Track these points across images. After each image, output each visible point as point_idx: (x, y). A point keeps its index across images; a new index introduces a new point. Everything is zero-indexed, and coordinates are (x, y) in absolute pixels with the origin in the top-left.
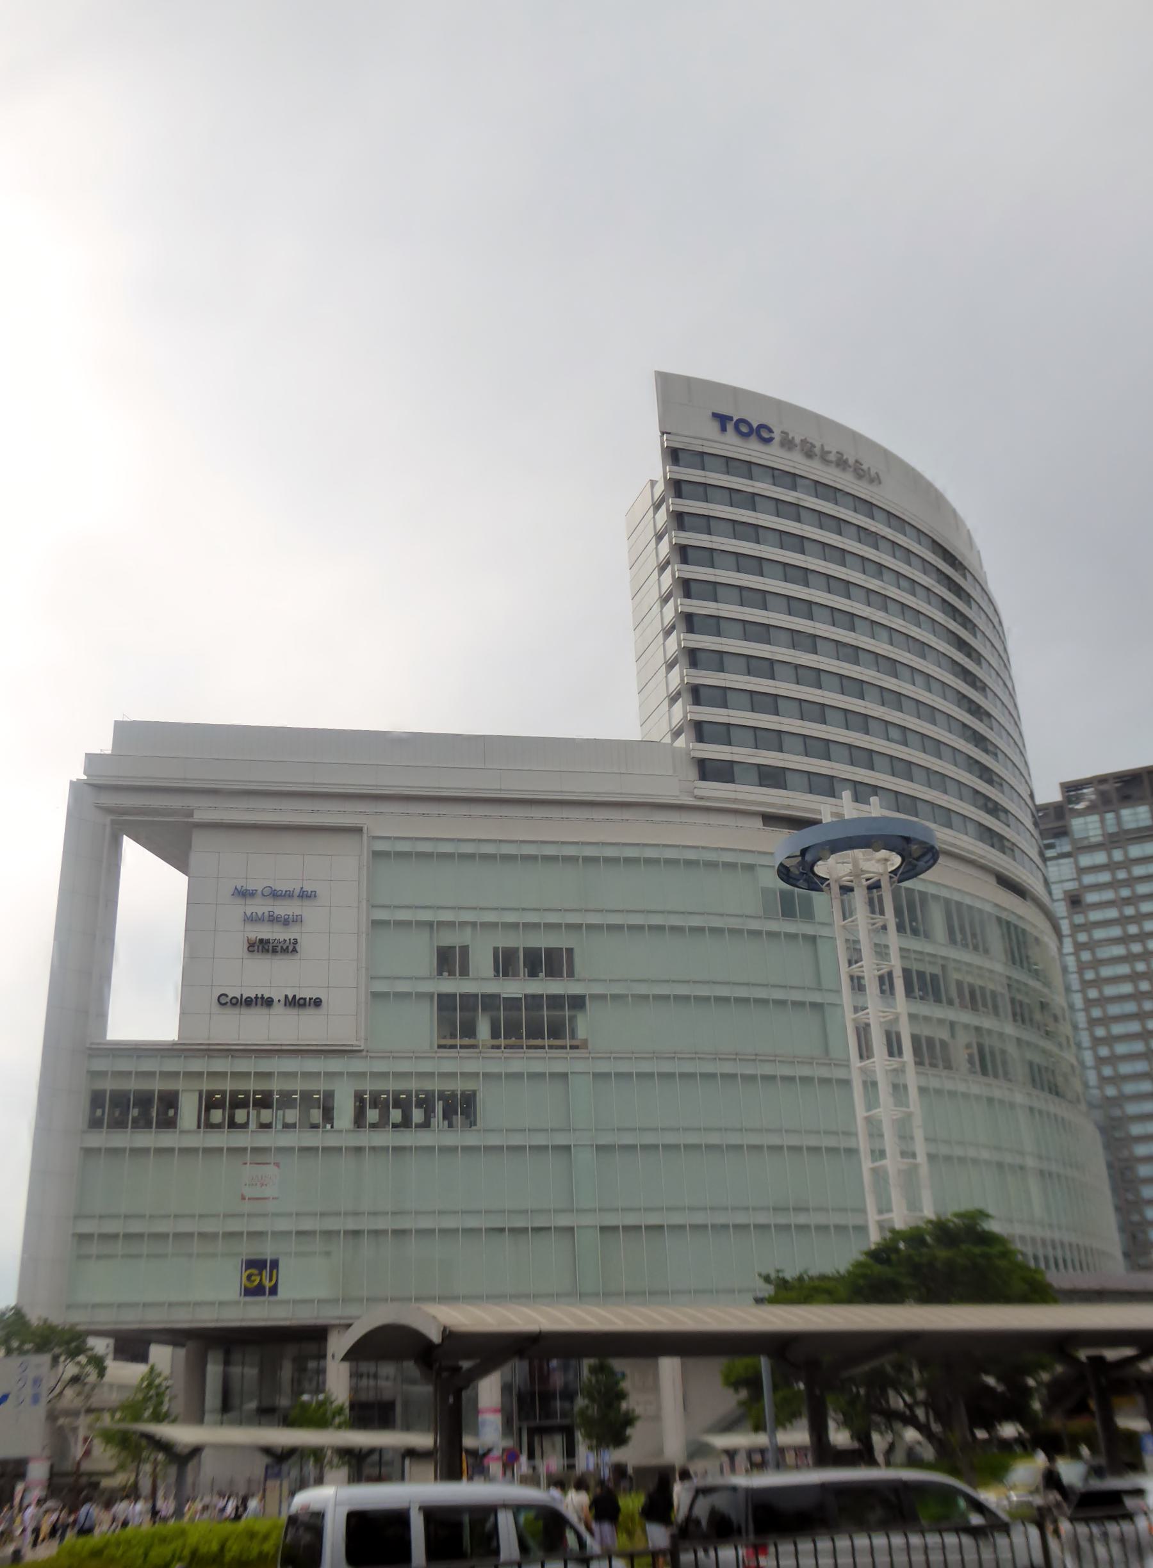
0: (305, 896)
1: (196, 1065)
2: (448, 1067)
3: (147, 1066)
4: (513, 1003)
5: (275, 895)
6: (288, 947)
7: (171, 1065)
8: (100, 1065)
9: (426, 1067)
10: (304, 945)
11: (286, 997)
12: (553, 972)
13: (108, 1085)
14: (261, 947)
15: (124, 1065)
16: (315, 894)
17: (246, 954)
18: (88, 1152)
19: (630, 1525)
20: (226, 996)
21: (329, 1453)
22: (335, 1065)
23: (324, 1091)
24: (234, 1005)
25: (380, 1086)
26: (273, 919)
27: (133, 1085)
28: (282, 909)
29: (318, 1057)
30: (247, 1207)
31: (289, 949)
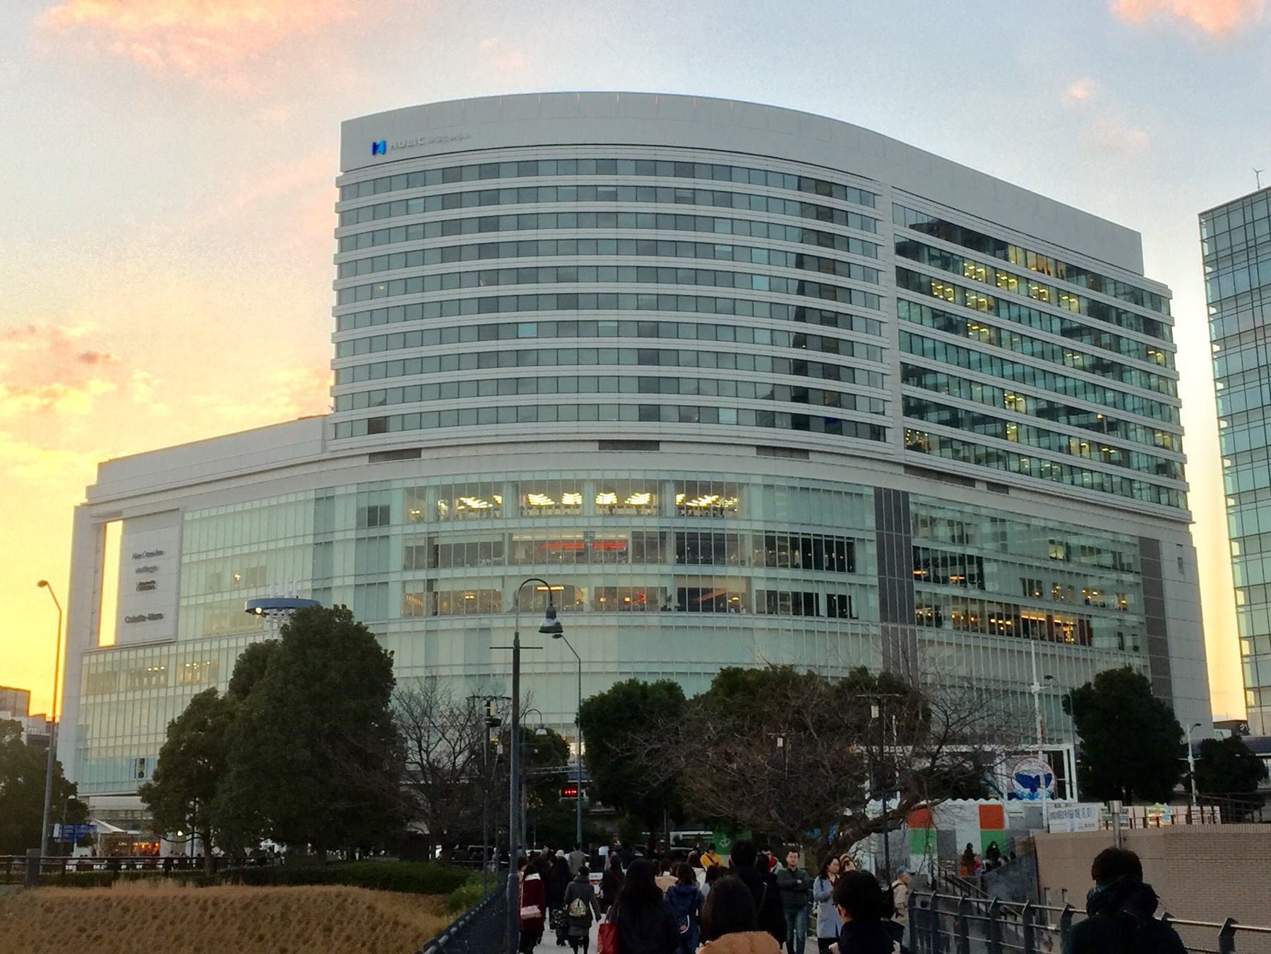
0: (160, 553)
5: (149, 555)
10: (159, 586)
19: (197, 515)
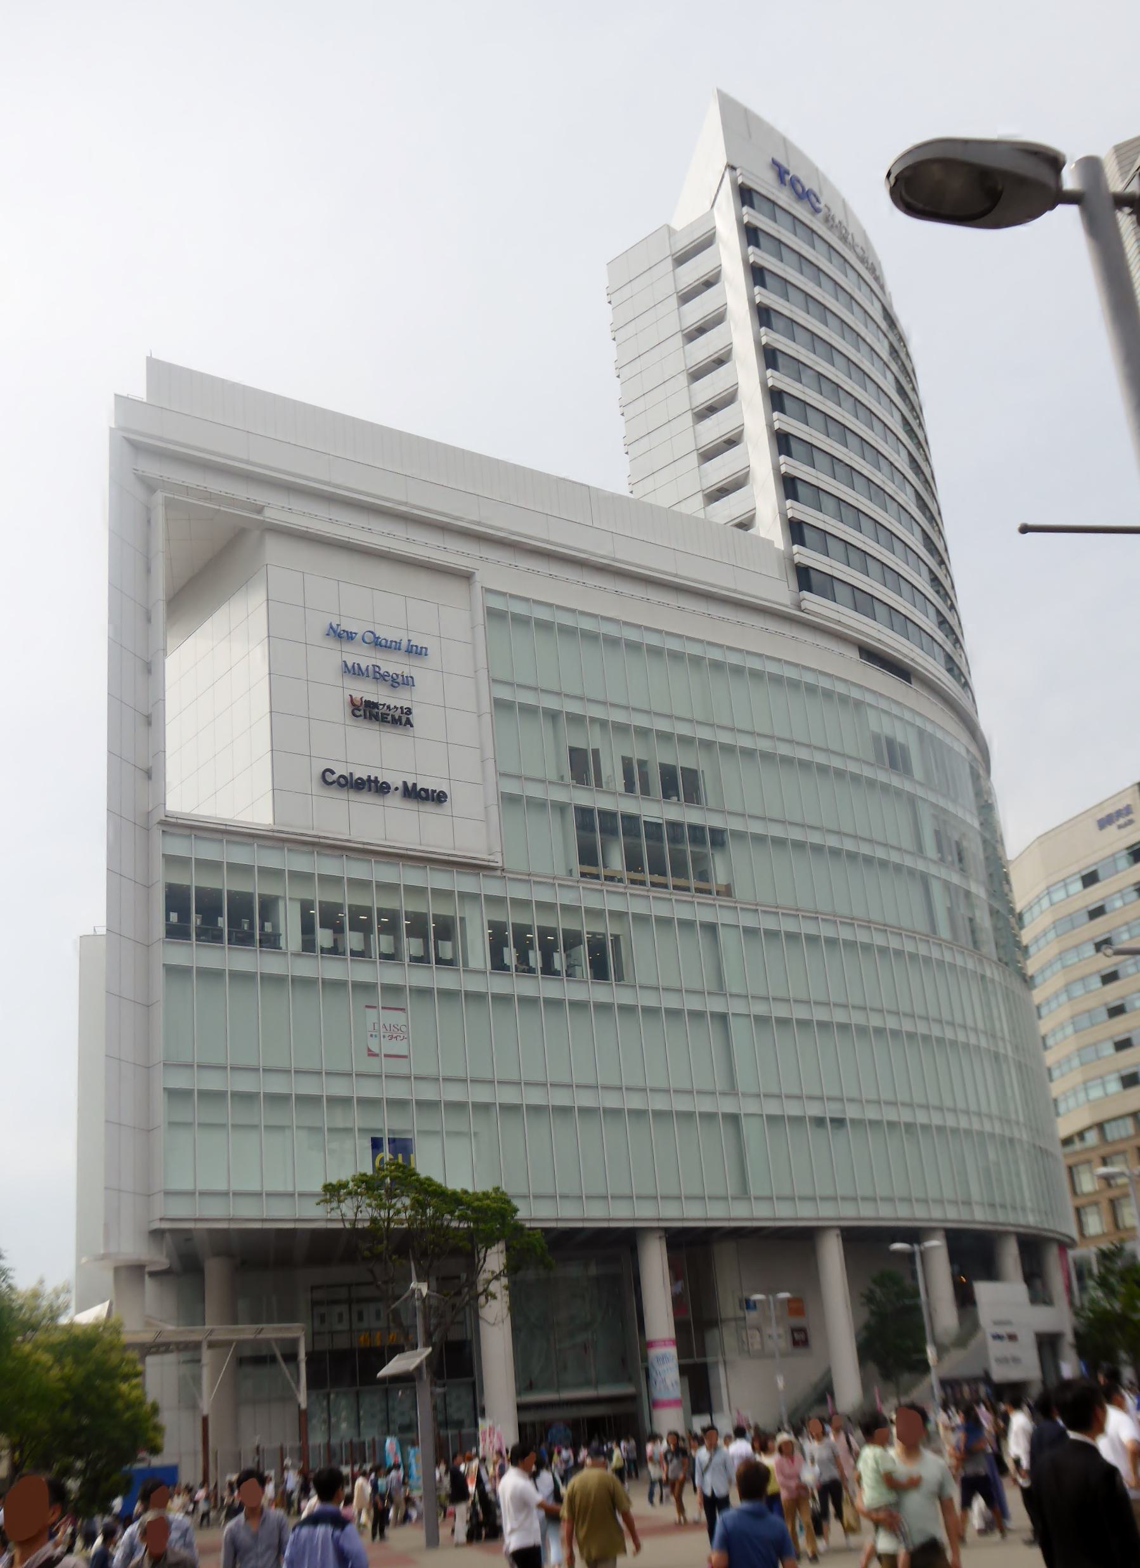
1: (300, 863)
2: (591, 901)
3: (240, 855)
4: (654, 830)
5: (377, 643)
6: (400, 717)
7: (272, 859)
8: (179, 847)
9: (566, 898)
11: (405, 783)
12: (693, 796)
13: (194, 880)
14: (367, 711)
15: (208, 851)
16: (426, 652)
17: (349, 719)
18: (173, 971)
20: (333, 773)
21: (519, 1399)
22: (465, 883)
23: (350, 906)
24: (342, 786)
25: (332, 896)
26: (379, 676)
27: (227, 884)
28: (392, 665)
29: (448, 871)
30: (372, 1065)
31: (400, 719)
